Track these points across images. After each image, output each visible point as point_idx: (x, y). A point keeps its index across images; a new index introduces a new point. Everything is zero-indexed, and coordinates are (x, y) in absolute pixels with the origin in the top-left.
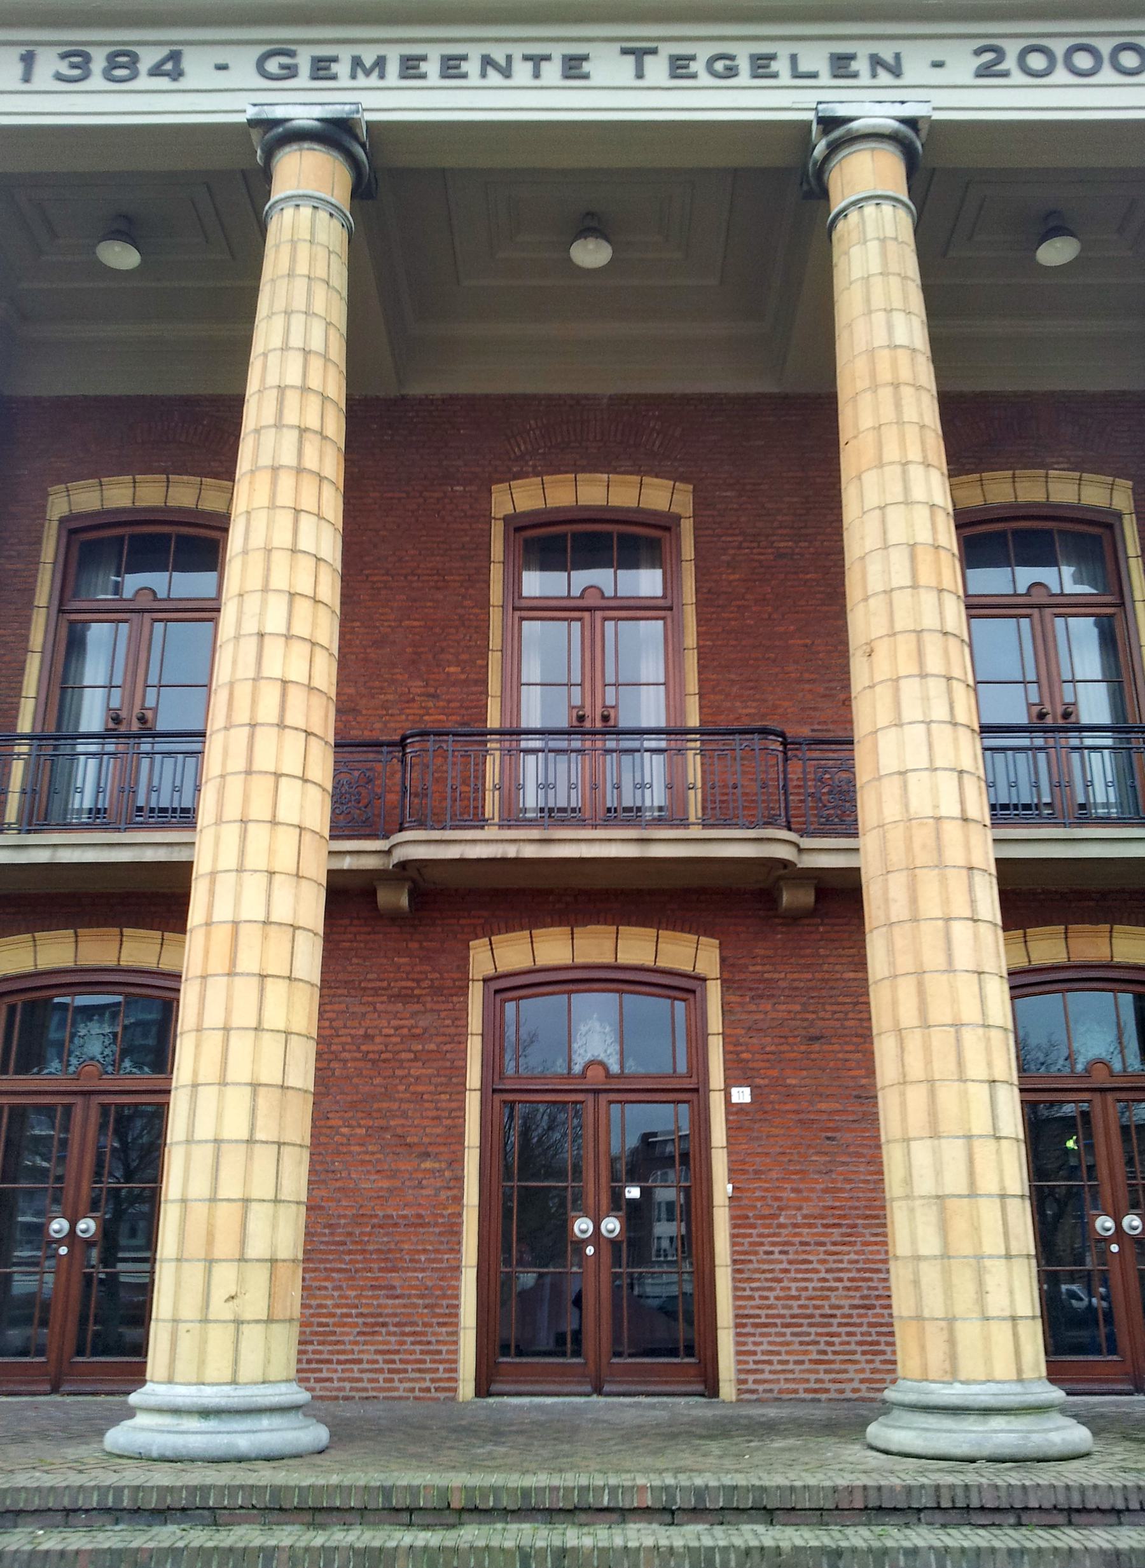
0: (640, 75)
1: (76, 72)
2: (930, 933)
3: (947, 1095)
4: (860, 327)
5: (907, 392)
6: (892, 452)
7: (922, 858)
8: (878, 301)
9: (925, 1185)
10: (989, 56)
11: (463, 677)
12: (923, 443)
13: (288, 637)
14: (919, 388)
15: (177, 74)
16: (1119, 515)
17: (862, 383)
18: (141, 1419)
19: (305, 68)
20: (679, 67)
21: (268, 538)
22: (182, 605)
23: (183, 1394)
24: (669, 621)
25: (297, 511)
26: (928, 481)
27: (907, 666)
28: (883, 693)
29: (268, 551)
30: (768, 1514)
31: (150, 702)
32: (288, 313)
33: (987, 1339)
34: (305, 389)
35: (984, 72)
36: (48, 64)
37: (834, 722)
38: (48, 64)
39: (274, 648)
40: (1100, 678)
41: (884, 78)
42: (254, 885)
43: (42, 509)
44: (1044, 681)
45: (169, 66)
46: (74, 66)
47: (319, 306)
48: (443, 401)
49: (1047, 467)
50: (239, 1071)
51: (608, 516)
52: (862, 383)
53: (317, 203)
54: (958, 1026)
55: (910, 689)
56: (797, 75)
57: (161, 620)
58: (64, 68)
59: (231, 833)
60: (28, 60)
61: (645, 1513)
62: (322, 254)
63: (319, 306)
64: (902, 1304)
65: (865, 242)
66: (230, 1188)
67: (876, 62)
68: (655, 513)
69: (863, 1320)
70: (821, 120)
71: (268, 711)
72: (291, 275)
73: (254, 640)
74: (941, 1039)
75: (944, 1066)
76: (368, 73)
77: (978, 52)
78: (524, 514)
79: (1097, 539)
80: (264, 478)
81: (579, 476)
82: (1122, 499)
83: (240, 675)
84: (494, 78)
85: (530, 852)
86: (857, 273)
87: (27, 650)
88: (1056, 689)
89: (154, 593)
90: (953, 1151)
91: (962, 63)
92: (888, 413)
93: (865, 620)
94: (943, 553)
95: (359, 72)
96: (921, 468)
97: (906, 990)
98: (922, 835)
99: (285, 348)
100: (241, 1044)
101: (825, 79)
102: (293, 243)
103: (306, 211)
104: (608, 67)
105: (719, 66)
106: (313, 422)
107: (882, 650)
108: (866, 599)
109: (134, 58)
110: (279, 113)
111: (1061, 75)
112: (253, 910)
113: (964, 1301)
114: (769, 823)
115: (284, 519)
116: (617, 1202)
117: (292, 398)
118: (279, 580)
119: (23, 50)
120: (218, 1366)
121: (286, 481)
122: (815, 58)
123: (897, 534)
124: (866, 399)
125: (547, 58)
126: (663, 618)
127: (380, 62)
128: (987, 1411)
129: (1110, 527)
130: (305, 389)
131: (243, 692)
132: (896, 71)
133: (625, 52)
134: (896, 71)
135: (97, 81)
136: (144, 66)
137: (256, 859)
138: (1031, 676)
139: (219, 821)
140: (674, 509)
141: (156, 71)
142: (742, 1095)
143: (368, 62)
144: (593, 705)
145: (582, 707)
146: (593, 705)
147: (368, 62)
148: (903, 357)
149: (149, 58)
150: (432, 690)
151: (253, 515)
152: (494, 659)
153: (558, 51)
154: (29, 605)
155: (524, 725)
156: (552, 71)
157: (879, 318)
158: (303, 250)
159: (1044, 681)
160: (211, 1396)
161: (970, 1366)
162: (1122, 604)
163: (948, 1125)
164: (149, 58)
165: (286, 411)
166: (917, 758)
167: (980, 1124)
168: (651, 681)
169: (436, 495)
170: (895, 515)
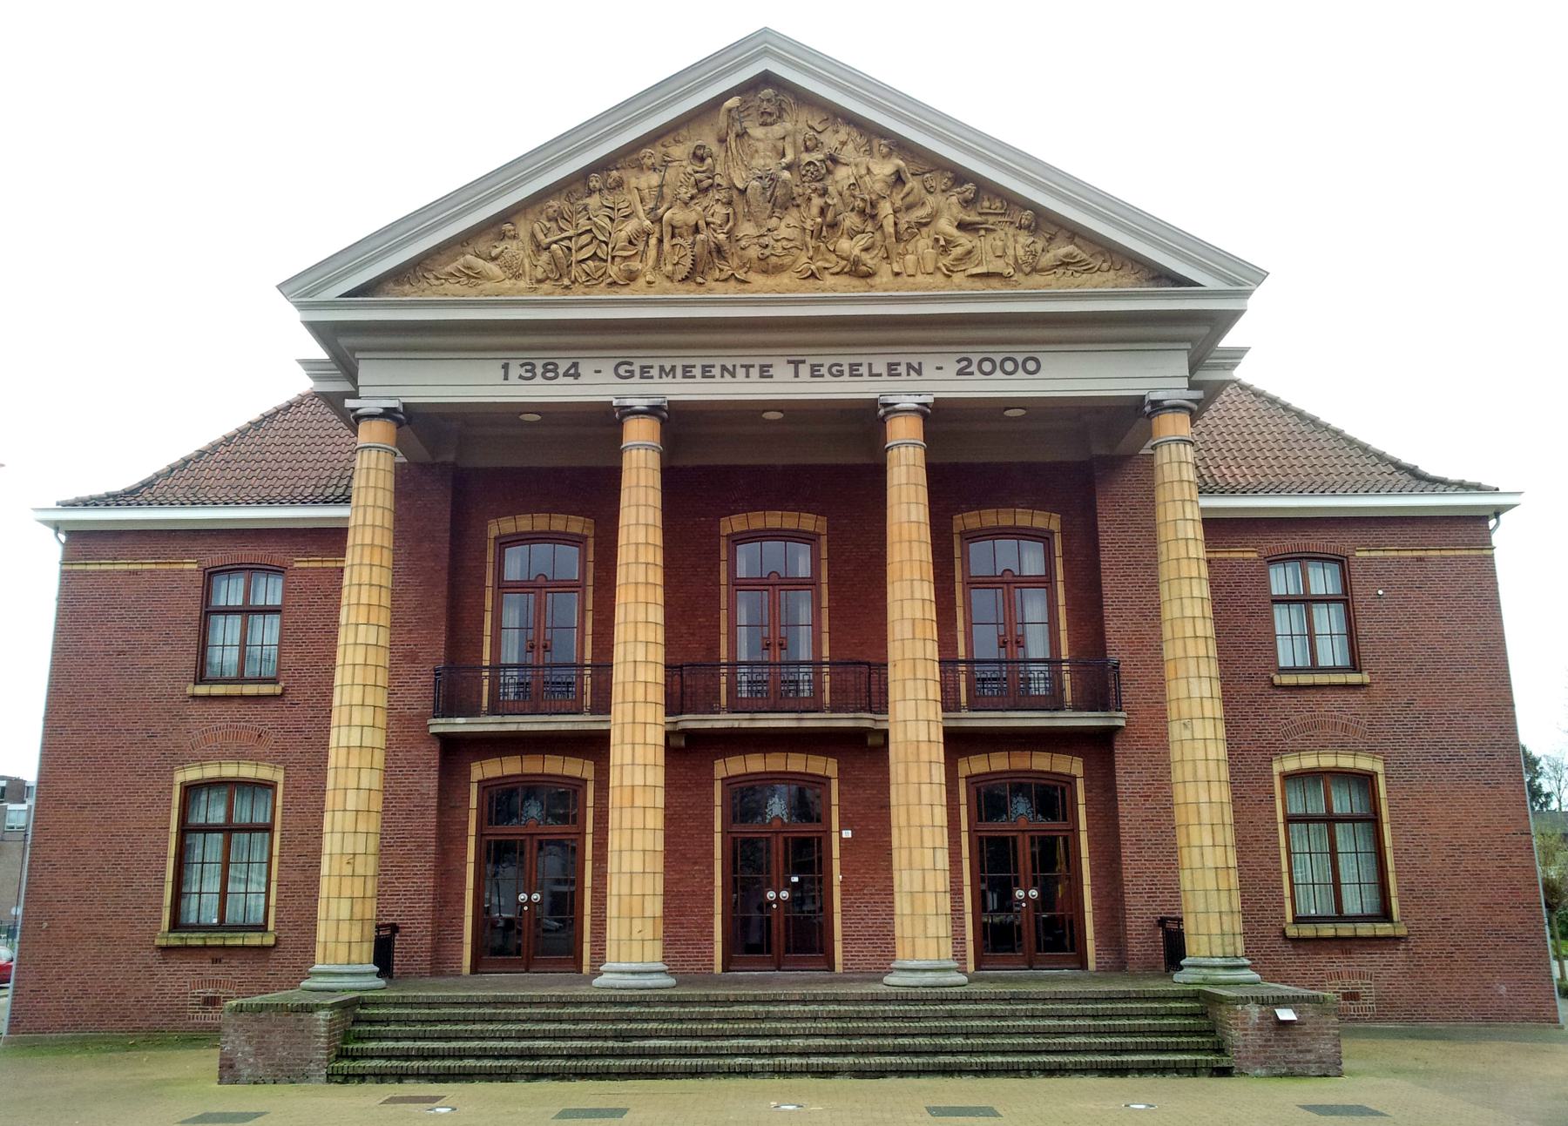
0: (797, 375)
2: (913, 789)
3: (916, 853)
6: (907, 575)
7: (911, 758)
9: (906, 888)
10: (965, 363)
15: (577, 376)
17: (896, 539)
18: (605, 976)
19: (637, 373)
20: (815, 371)
23: (616, 966)
27: (909, 675)
28: (899, 685)
30: (839, 1002)
33: (927, 946)
35: (960, 372)
36: (516, 371)
38: (516, 371)
41: (913, 375)
42: (639, 771)
43: (485, 532)
47: (651, 502)
49: (1014, 506)
50: (638, 845)
52: (896, 539)
53: (647, 447)
54: (921, 826)
55: (910, 684)
56: (871, 375)
58: (522, 372)
59: (628, 748)
60: (506, 367)
61: (796, 1002)
64: (898, 933)
66: (637, 891)
69: (882, 940)
71: (640, 696)
72: (638, 486)
74: (915, 831)
75: (915, 842)
84: (728, 377)
85: (745, 725)
90: (917, 875)
91: (952, 367)
92: (906, 556)
93: (894, 652)
97: (903, 810)
98: (912, 749)
100: (638, 835)
101: (885, 377)
103: (642, 452)
104: (782, 370)
107: (899, 665)
112: (639, 781)
113: (919, 930)
114: (863, 710)
115: (642, 607)
116: (788, 885)
117: (642, 548)
118: (641, 637)
120: (637, 956)
121: (641, 589)
123: (907, 614)
124: (897, 546)
127: (673, 368)
128: (925, 970)
131: (629, 687)
132: (919, 372)
134: (919, 372)
135: (539, 379)
136: (561, 371)
137: (639, 760)
139: (622, 743)
141: (566, 374)
142: (847, 834)
149: (563, 366)
152: (723, 613)
153: (758, 362)
156: (755, 372)
157: (904, 506)
158: (642, 472)
160: (634, 967)
161: (920, 954)
163: (916, 864)
164: (563, 366)
166: (911, 715)
167: (928, 864)
170: (907, 604)
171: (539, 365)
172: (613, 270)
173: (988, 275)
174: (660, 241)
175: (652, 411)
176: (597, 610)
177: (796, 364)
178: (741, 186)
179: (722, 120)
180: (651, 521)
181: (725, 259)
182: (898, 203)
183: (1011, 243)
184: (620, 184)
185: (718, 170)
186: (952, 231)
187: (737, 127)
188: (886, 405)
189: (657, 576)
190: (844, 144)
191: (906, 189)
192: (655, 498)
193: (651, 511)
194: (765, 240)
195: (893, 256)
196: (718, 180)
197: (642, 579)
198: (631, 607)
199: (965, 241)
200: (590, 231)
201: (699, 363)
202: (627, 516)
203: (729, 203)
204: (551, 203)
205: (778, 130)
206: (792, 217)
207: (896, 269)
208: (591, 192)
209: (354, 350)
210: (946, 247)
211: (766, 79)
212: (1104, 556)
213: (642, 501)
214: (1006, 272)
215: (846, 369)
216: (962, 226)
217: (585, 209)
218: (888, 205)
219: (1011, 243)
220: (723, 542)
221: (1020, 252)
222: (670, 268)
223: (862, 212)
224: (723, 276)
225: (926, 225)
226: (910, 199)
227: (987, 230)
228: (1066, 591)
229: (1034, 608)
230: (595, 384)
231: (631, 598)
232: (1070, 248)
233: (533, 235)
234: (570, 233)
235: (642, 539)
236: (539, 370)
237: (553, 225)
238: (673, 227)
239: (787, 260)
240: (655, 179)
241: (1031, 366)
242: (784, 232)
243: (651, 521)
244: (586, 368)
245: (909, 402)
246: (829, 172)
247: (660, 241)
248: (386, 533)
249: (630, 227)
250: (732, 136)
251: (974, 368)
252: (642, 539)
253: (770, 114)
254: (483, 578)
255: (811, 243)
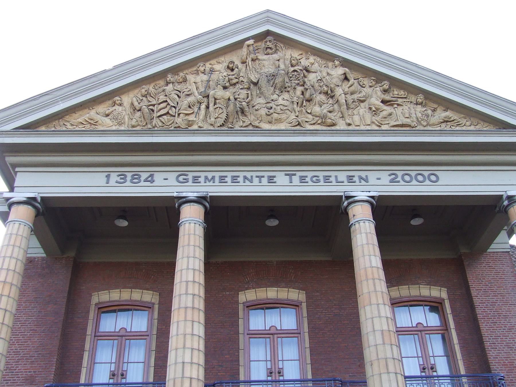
1: (122, 180)
4: (361, 260)
5: (377, 281)
6: (374, 301)
8: (366, 253)
10: (393, 176)
11: (231, 359)
12: (383, 298)
13: (192, 363)
14: (380, 280)
15: (152, 181)
16: (444, 300)
17: (363, 278)
19: (191, 180)
20: (302, 179)
21: (185, 331)
22: (135, 334)
24: (299, 338)
25: (193, 321)
26: (385, 309)
27: (384, 370)
29: (185, 335)
31: (125, 369)
32: (188, 257)
34: (194, 282)
35: (392, 181)
36: (114, 177)
37: (356, 373)
38: (114, 177)
39: (188, 367)
40: (443, 355)
41: (363, 183)
44: (424, 356)
45: (150, 179)
46: (121, 179)
47: (197, 255)
48: (222, 263)
51: (277, 302)
57: (129, 339)
58: (118, 179)
60: (108, 177)
62: (197, 237)
63: (197, 255)
65: (361, 233)
67: (361, 178)
68: (293, 301)
70: (345, 197)
72: (189, 245)
73: (181, 365)
76: (210, 181)
77: (390, 175)
78: (249, 301)
79: (437, 307)
80: (182, 311)
81: (268, 289)
82: (444, 295)
83: (177, 376)
86: (359, 243)
87: (84, 351)
88: (428, 359)
89: (126, 329)
91: (385, 177)
92: (372, 288)
93: (370, 354)
94: (391, 332)
95: (207, 181)
96: (383, 305)
99: (188, 269)
101: (346, 183)
102: (189, 235)
104: (281, 179)
105: (314, 179)
106: (197, 292)
108: (369, 347)
109: (140, 176)
110: (184, 195)
111: (414, 182)
115: (189, 324)
118: (188, 345)
119: (107, 174)
121: (189, 312)
122: (342, 176)
125: (263, 177)
126: (297, 337)
127: (213, 178)
129: (441, 303)
130: (194, 282)
132: (366, 180)
133: (286, 175)
134: (366, 180)
135: (128, 183)
136: (143, 179)
138: (420, 355)
140: (300, 299)
141: (146, 181)
143: (210, 178)
144: (275, 368)
145: (271, 368)
146: (275, 368)
147: (210, 178)
148: (375, 270)
150: (220, 364)
151: (179, 323)
154: (85, 334)
155: (253, 379)
158: (192, 237)
159: (424, 356)
162: (447, 330)
164: (144, 176)
165: (189, 289)
168: (293, 359)
169: (221, 295)
171: (129, 176)
172: (179, 121)
173: (402, 126)
174: (208, 107)
175: (200, 200)
176: (157, 351)
177: (291, 176)
178: (255, 81)
179: (245, 50)
180: (197, 267)
181: (246, 116)
182: (346, 90)
183: (413, 111)
184: (185, 80)
185: (241, 74)
186: (378, 103)
187: (252, 56)
188: (348, 198)
189: (200, 304)
190: (312, 64)
191: (351, 83)
192: (200, 253)
193: (197, 261)
194: (269, 105)
195: (346, 115)
196: (241, 79)
197: (190, 304)
198: (182, 324)
199: (388, 109)
200: (166, 101)
201: (229, 175)
202: (178, 288)
203: (249, 88)
204: (144, 86)
205: (276, 56)
206: (286, 96)
207: (349, 122)
208: (167, 84)
209: (15, 166)
210: (376, 112)
211: (268, 33)
212: (478, 311)
213: (192, 254)
214: (412, 124)
215: (321, 178)
216: (383, 102)
217: (164, 91)
218: (341, 90)
219: (413, 111)
220: (241, 307)
221: (419, 115)
222: (213, 119)
223: (326, 93)
224: (245, 125)
225: (363, 101)
226: (352, 88)
227: (398, 105)
228: (458, 334)
229: (436, 346)
230: (164, 184)
231: (182, 318)
232: (448, 113)
233: (132, 104)
234: (154, 102)
235: (191, 279)
236: (129, 178)
237: (144, 98)
238: (215, 99)
239: (284, 116)
240: (205, 77)
241: (433, 178)
242: (280, 101)
243: (197, 267)
244: (159, 178)
245: (363, 196)
246: (305, 76)
247: (208, 107)
248: (16, 275)
249: (191, 99)
250: (249, 59)
251: (399, 179)
252: (190, 304)
253: (271, 48)
254: (86, 329)
255: (297, 109)
